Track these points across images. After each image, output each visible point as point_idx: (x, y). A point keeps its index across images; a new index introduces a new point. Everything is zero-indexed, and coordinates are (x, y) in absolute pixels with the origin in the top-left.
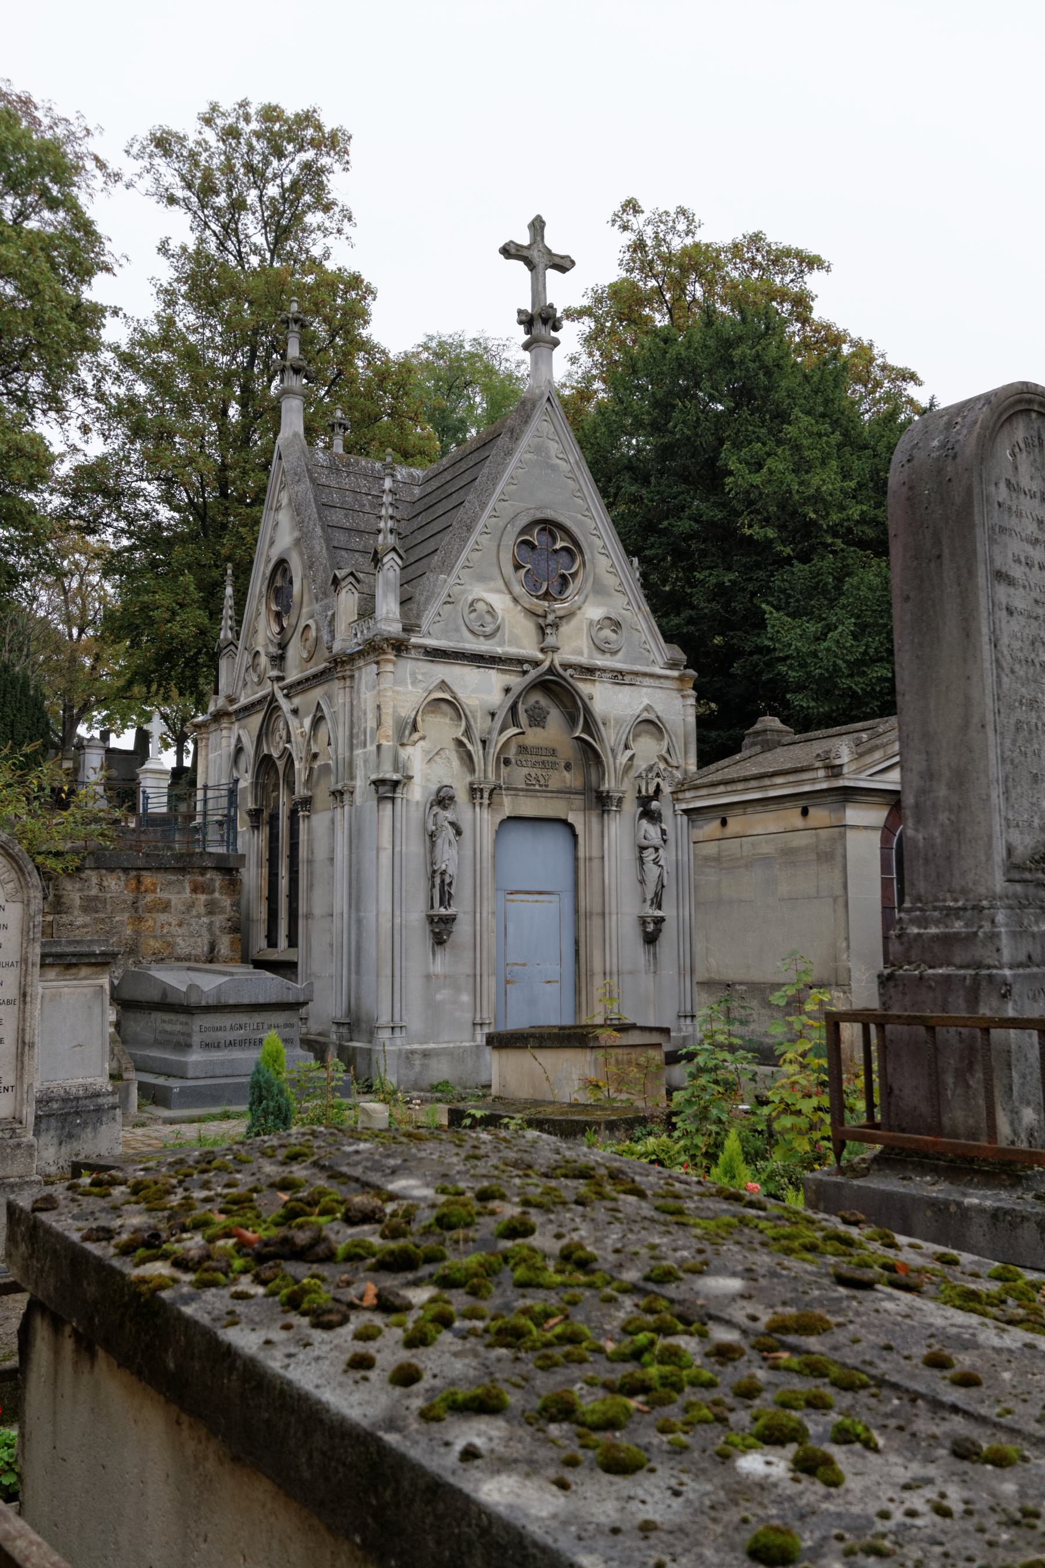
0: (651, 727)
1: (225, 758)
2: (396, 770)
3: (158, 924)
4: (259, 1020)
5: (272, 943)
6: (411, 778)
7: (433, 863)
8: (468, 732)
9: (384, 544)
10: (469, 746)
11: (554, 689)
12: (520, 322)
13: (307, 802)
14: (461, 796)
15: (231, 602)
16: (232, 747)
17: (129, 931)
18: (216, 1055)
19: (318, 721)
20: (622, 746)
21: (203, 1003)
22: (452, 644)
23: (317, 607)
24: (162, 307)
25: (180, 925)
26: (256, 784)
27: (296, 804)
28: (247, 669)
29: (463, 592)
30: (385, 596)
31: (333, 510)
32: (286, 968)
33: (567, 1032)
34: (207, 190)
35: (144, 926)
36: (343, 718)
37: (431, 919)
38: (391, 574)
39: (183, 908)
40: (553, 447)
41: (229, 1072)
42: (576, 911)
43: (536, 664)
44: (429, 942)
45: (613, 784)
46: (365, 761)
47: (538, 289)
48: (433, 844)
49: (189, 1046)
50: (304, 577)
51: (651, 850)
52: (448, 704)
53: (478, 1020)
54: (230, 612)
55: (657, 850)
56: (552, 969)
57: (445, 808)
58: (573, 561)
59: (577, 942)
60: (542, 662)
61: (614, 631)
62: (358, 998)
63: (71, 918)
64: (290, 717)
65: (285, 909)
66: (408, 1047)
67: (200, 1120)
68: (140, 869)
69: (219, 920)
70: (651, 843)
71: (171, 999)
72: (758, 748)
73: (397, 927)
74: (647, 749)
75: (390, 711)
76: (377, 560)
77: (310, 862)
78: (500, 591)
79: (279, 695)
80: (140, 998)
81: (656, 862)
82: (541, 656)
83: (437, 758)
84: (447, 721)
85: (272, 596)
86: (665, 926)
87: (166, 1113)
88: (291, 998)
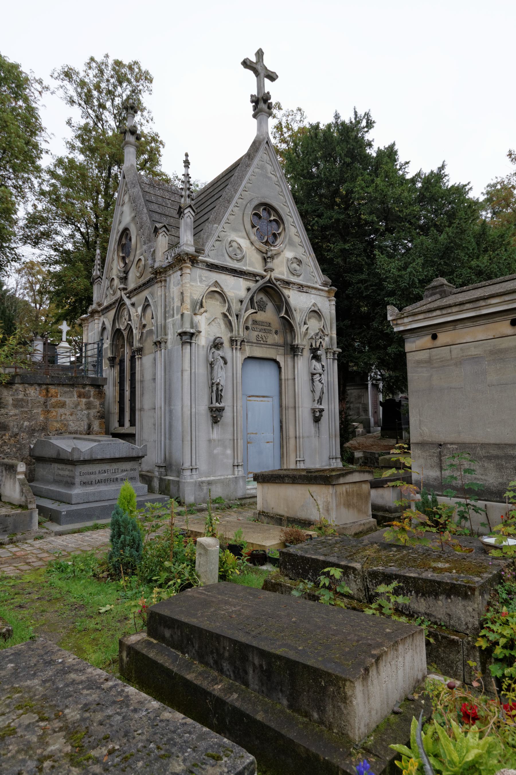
0: (315, 314)
1: (96, 334)
2: (192, 327)
3: (59, 414)
4: (115, 467)
5: (121, 424)
6: (200, 332)
7: (212, 379)
8: (229, 310)
10: (230, 318)
11: (271, 292)
13: (140, 350)
15: (99, 257)
16: (100, 328)
17: (42, 418)
18: (90, 489)
19: (146, 306)
21: (82, 459)
23: (145, 247)
24: (69, 151)
25: (71, 415)
26: (112, 345)
27: (134, 352)
28: (107, 289)
32: (130, 437)
35: (50, 415)
37: (211, 410)
40: (269, 168)
41: (98, 499)
42: (281, 406)
43: (263, 277)
44: (210, 422)
45: (300, 341)
46: (173, 325)
47: (260, 86)
48: (212, 368)
49: (73, 484)
50: (138, 235)
51: (318, 375)
52: (220, 294)
53: (236, 464)
54: (99, 262)
55: (320, 375)
57: (218, 349)
58: (279, 228)
59: (281, 422)
60: (266, 276)
61: (298, 265)
62: (170, 453)
63: (7, 411)
64: (130, 307)
65: (128, 406)
66: (199, 479)
67: (79, 531)
68: (48, 384)
69: (93, 412)
70: (317, 372)
72: (438, 296)
73: (193, 413)
74: (314, 325)
75: (189, 295)
76: (180, 212)
77: (142, 382)
78: (245, 238)
79: (125, 298)
80: (46, 456)
81: (320, 381)
82: (265, 273)
83: (213, 323)
84: (218, 303)
85: (120, 249)
87: (57, 528)
88: (134, 454)
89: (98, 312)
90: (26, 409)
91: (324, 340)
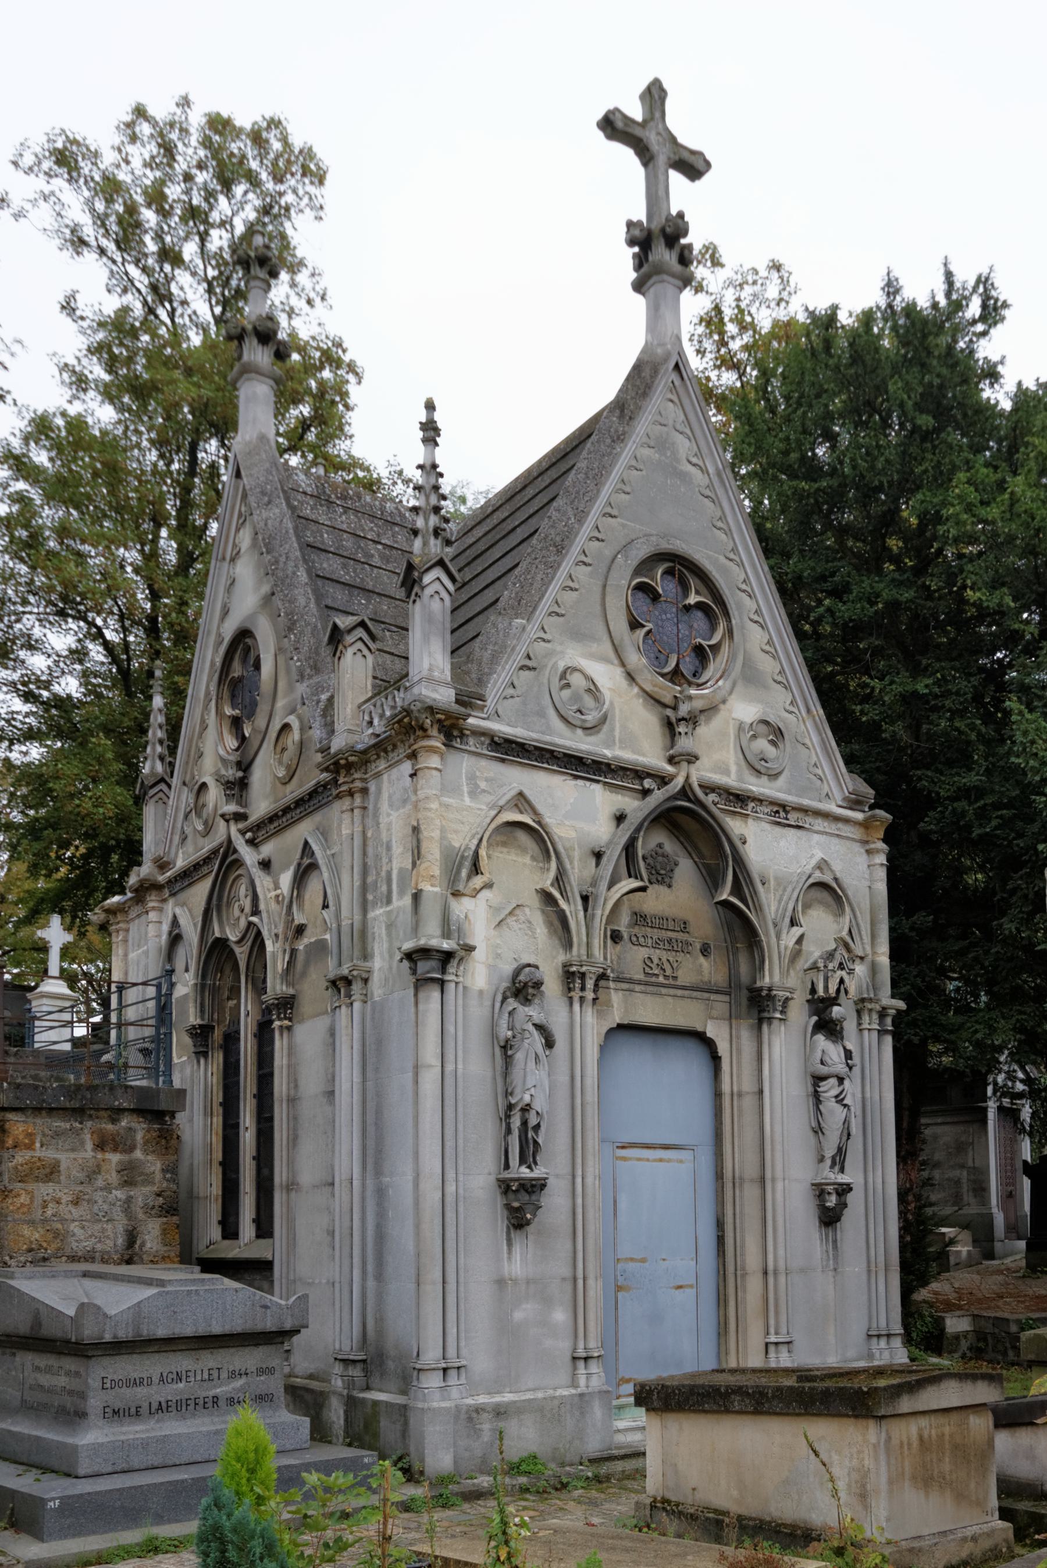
0: (825, 895)
1: (153, 954)
2: (446, 934)
3: (38, 1201)
5: (230, 1231)
6: (470, 949)
7: (508, 1093)
8: (560, 880)
9: (424, 554)
11: (688, 825)
12: (631, 242)
13: (287, 1005)
14: (552, 986)
15: (161, 719)
16: (164, 937)
18: (134, 1431)
19: (305, 871)
20: (787, 920)
21: (108, 1337)
22: (534, 735)
23: (302, 688)
25: (76, 1203)
26: (201, 987)
28: (186, 816)
29: (550, 654)
30: (426, 639)
31: (323, 555)
32: (255, 1271)
33: (820, 1385)
34: (128, 234)
36: (349, 860)
37: (505, 1187)
38: (436, 605)
39: (81, 1176)
40: (683, 446)
42: (719, 1176)
43: (663, 780)
44: (502, 1225)
45: (777, 978)
46: (390, 926)
47: (656, 194)
48: (508, 1060)
50: (280, 650)
52: (530, 832)
53: (581, 1353)
54: (160, 734)
55: (841, 1080)
56: (684, 1267)
57: (527, 1001)
59: (720, 1225)
61: (773, 743)
62: (380, 1320)
64: (257, 874)
65: (251, 1175)
66: (470, 1401)
69: (143, 1194)
71: (46, 1331)
73: (450, 1199)
74: (821, 929)
75: (436, 834)
76: (410, 581)
78: (606, 660)
79: (240, 844)
81: (839, 1099)
82: (670, 769)
83: (511, 921)
84: (527, 860)
85: (226, 694)
86: (850, 1198)
88: (269, 1324)
91: (851, 972)
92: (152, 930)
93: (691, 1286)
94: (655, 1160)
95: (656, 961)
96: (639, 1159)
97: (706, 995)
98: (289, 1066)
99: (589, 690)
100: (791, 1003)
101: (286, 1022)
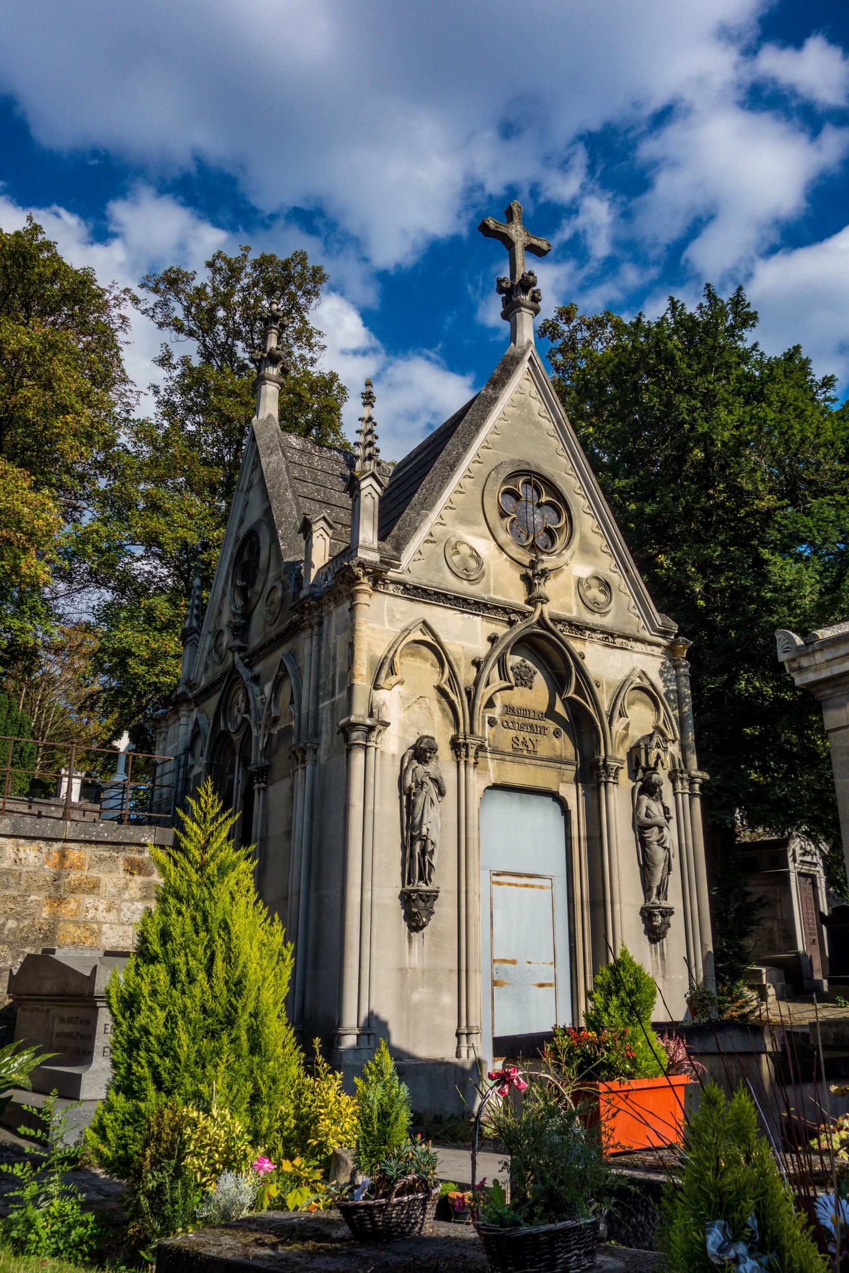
6: (387, 725)
10: (453, 696)
11: (544, 649)
14: (444, 751)
25: (109, 910)
28: (209, 653)
43: (524, 615)
60: (531, 613)
68: (65, 841)
73: (367, 903)
78: (482, 536)
82: (531, 608)
84: (428, 666)
89: (188, 701)
90: (15, 893)
91: (665, 750)
92: (182, 730)
93: (551, 985)
94: (522, 886)
95: (521, 739)
96: (510, 884)
97: (558, 765)
98: (263, 815)
99: (472, 556)
100: (621, 772)
101: (263, 785)
